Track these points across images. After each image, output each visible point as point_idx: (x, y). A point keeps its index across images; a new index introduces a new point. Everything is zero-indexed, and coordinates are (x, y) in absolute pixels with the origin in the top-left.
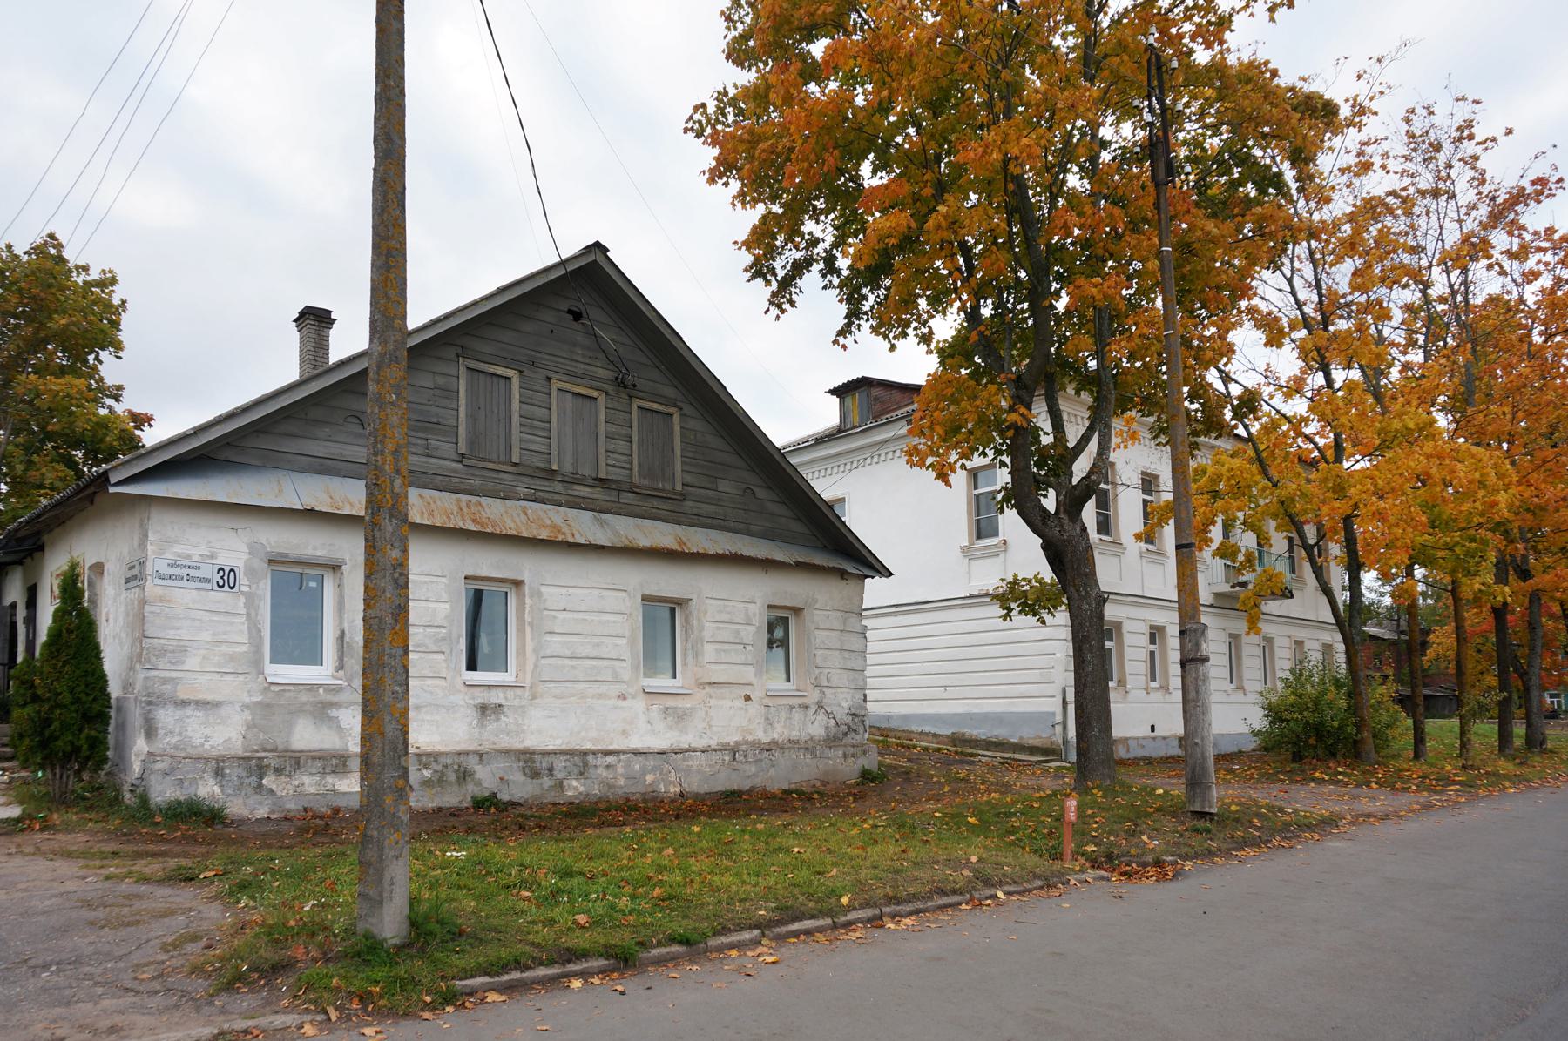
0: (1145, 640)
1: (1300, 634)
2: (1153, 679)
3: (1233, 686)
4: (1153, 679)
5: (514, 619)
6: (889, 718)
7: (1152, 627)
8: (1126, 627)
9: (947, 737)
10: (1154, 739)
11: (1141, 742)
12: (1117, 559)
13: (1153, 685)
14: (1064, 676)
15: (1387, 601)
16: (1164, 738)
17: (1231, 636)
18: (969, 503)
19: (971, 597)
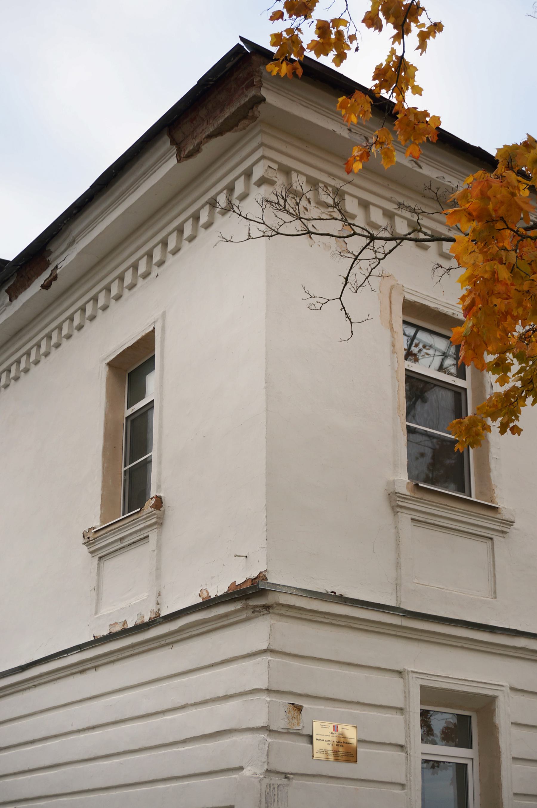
12: (482, 547)
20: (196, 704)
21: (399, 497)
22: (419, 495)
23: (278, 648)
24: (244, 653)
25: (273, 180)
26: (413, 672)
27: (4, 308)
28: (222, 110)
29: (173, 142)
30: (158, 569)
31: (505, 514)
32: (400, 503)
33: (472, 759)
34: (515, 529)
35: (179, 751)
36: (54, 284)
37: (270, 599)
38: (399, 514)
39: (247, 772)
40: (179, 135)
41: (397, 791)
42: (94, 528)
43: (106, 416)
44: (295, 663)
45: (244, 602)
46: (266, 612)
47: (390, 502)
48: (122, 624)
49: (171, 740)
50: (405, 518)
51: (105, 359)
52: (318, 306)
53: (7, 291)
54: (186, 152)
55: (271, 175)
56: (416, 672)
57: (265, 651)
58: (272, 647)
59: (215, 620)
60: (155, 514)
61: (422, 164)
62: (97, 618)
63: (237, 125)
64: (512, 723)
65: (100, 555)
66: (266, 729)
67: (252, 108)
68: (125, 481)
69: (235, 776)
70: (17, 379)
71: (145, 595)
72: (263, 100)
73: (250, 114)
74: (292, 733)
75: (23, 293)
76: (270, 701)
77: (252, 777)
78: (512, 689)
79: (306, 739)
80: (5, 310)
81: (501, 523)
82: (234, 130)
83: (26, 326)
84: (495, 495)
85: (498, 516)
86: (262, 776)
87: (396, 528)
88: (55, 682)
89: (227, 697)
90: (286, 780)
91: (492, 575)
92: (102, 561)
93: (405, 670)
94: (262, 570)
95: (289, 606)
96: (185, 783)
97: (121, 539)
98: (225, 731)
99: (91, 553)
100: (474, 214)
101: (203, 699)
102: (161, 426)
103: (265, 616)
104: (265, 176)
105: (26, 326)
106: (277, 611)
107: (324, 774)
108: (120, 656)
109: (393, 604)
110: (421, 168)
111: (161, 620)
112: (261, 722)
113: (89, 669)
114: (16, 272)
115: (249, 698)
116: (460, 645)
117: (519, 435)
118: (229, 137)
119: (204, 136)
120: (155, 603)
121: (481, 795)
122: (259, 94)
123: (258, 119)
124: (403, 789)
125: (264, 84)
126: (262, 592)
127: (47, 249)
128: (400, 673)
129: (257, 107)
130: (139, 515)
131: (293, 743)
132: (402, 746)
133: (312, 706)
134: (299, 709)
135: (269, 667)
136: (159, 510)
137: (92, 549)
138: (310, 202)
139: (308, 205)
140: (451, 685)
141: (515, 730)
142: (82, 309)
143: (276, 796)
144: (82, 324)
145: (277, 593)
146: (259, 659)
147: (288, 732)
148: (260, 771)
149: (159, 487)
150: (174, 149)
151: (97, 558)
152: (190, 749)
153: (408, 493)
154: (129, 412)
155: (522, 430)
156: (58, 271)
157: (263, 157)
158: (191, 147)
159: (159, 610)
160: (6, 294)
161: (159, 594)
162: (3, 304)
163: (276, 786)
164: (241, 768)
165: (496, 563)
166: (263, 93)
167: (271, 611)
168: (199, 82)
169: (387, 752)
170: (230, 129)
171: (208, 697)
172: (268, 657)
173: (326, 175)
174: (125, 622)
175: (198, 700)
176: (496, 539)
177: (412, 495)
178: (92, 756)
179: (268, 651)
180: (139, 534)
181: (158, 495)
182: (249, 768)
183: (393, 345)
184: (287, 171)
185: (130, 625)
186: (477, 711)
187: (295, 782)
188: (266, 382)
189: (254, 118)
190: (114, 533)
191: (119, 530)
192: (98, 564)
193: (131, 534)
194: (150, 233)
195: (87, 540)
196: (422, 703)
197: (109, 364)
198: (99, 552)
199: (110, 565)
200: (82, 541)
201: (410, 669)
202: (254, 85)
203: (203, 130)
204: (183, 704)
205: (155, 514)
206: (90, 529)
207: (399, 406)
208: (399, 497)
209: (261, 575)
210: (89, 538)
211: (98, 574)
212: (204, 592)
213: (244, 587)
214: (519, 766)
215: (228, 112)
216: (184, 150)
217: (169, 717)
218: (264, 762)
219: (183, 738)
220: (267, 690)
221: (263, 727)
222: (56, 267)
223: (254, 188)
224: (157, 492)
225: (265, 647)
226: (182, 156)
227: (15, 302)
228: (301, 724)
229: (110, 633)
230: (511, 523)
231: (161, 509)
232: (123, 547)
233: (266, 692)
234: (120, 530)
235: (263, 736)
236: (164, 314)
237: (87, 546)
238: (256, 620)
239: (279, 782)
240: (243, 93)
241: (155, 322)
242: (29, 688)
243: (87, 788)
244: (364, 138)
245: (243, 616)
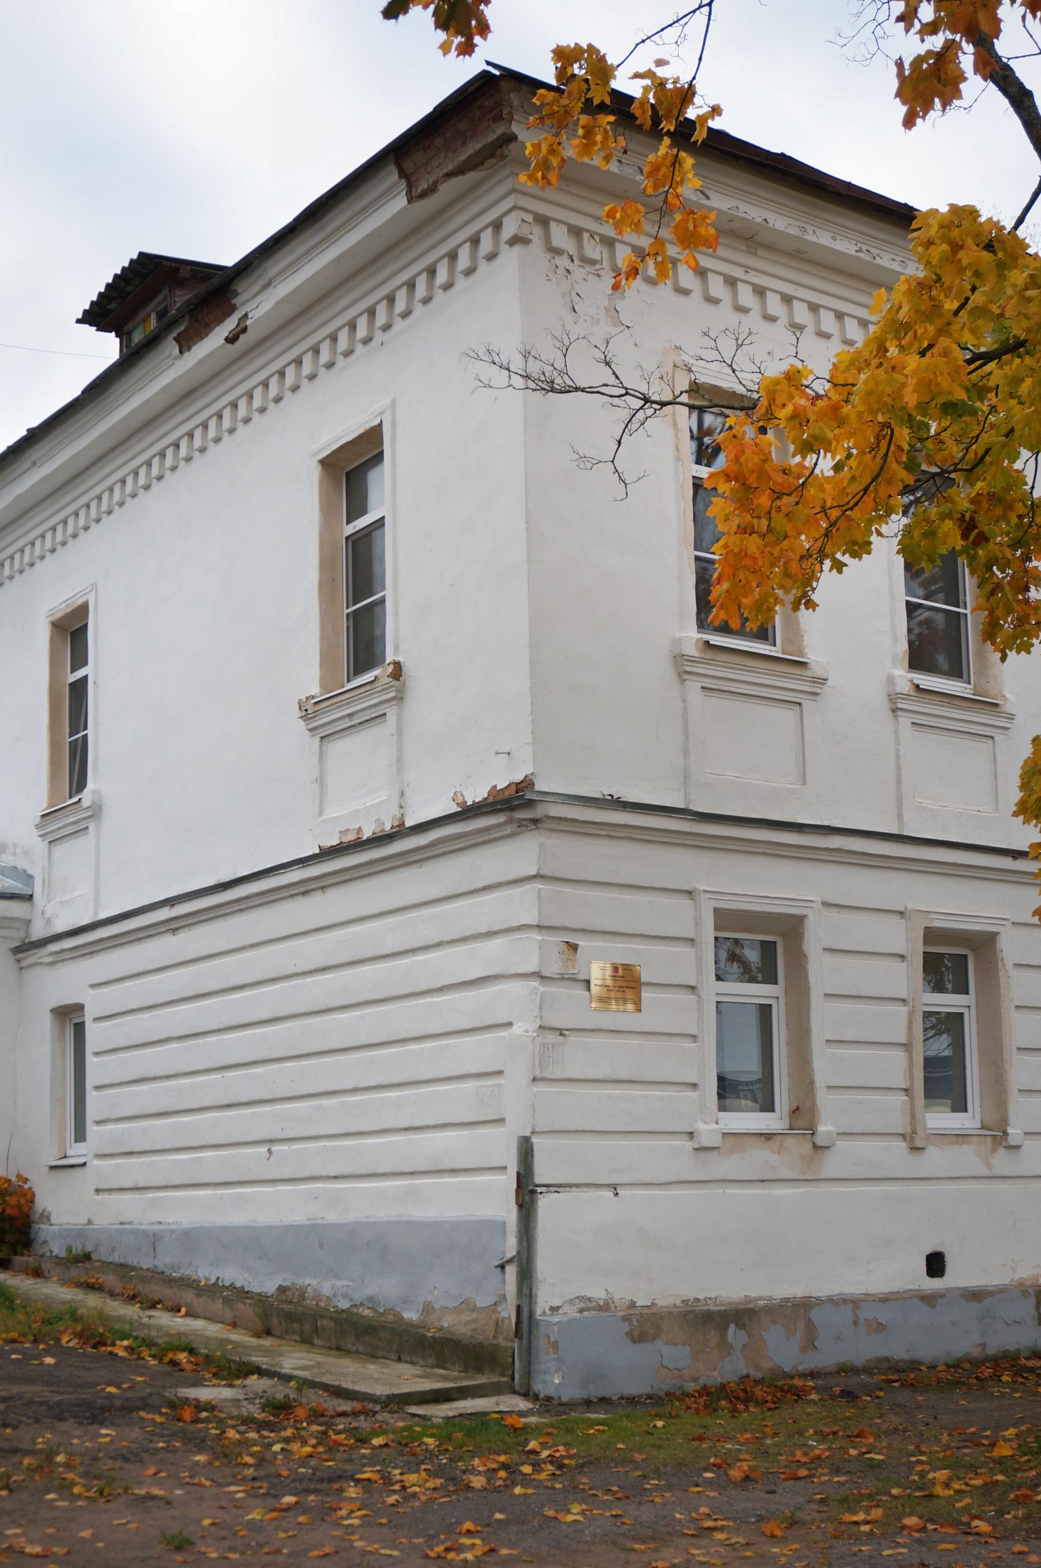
6: (154, 1240)
7: (931, 935)
9: (261, 1299)
10: (929, 1299)
11: (867, 1313)
12: (787, 716)
15: (707, 514)
16: (975, 1295)
18: (326, 565)
19: (327, 853)
20: (453, 942)
21: (687, 660)
22: (710, 655)
23: (549, 874)
24: (510, 878)
25: (527, 238)
26: (705, 891)
27: (171, 363)
28: (464, 144)
29: (403, 174)
30: (399, 760)
31: (816, 671)
32: (688, 669)
33: (777, 998)
34: (830, 687)
35: (435, 1002)
36: (242, 337)
37: (538, 812)
38: (687, 682)
39: (517, 1029)
40: (408, 166)
41: (688, 1045)
42: (313, 697)
43: (321, 535)
44: (569, 890)
45: (508, 814)
46: (534, 827)
47: (676, 666)
48: (355, 832)
49: (424, 988)
50: (694, 686)
51: (316, 454)
52: (589, 466)
53: (175, 339)
54: (419, 191)
55: (524, 233)
56: (709, 892)
57: (534, 877)
58: (542, 872)
59: (474, 834)
60: (393, 686)
61: (709, 193)
62: (323, 821)
63: (482, 163)
64: (825, 949)
65: (322, 735)
66: (538, 975)
67: (501, 146)
68: (348, 627)
69: (503, 1033)
70: (188, 459)
71: (383, 795)
72: (514, 138)
73: (498, 152)
74: (567, 979)
75: (198, 344)
76: (543, 940)
77: (523, 1035)
78: (826, 904)
79: (582, 985)
80: (173, 364)
81: (812, 682)
82: (479, 169)
83: (201, 386)
84: (805, 643)
85: (808, 673)
86: (535, 1034)
87: (684, 701)
88: (268, 906)
89: (491, 934)
90: (561, 1037)
91: (801, 753)
92: (325, 742)
93: (695, 889)
94: (529, 772)
95: (560, 819)
96: (444, 1042)
97: (350, 715)
98: (489, 976)
99: (311, 730)
100: (732, 475)
101: (462, 936)
102: (395, 563)
103: (532, 832)
104: (519, 234)
105: (201, 386)
106: (549, 826)
107: (604, 1028)
108: (355, 875)
109: (680, 805)
110: (709, 199)
111: (407, 831)
112: (532, 967)
113: (313, 890)
114: (188, 312)
115: (517, 936)
116: (761, 850)
117: (814, 611)
118: (471, 176)
119: (441, 175)
120: (397, 806)
121: (788, 1044)
122: (509, 131)
123: (508, 158)
124: (695, 1042)
125: (515, 117)
126: (530, 804)
127: (232, 288)
128: (689, 893)
129: (508, 146)
130: (373, 686)
131: (568, 991)
132: (693, 988)
133: (588, 944)
134: (574, 947)
135: (539, 897)
136: (398, 680)
137: (311, 726)
138: (572, 261)
139: (571, 264)
140: (750, 905)
141: (829, 959)
142: (279, 373)
143: (551, 1059)
144: (280, 395)
145: (546, 804)
146: (528, 886)
147: (563, 978)
148: (532, 1027)
149: (396, 648)
150: (403, 184)
151: (318, 738)
152: (448, 1000)
153: (697, 655)
154: (350, 529)
155: (818, 606)
156: (248, 322)
157: (515, 208)
158: (425, 186)
159: (402, 815)
160: (175, 343)
161: (403, 794)
162: (170, 356)
163: (550, 1046)
164: (510, 1024)
165: (806, 737)
166: (515, 128)
167: (539, 825)
168: (435, 109)
169: (676, 996)
170: (474, 168)
171: (468, 934)
172: (537, 885)
173: (592, 220)
174: (359, 830)
175: (456, 937)
176: (804, 703)
177: (702, 656)
178: (324, 1007)
179: (538, 877)
180: (373, 710)
181: (397, 659)
182: (519, 1024)
183: (677, 450)
184: (544, 221)
185: (366, 834)
186: (784, 935)
187: (573, 1039)
188: (527, 523)
189: (503, 157)
190: (340, 707)
191: (347, 704)
192: (321, 746)
193: (363, 710)
194: (370, 284)
195: (304, 713)
196: (716, 929)
197: (323, 462)
198: (321, 730)
199: (337, 748)
200: (297, 713)
201: (701, 888)
202: (504, 119)
203: (440, 164)
204: (437, 941)
205: (393, 686)
206: (307, 698)
207: (685, 534)
208: (687, 660)
209: (527, 779)
210: (306, 710)
211: (321, 759)
212: (459, 795)
213: (507, 793)
214: (832, 1004)
215: (473, 147)
216: (417, 187)
217: (420, 957)
218: (536, 1017)
219: (439, 985)
220: (538, 926)
221: (534, 973)
222: (246, 316)
223: (504, 248)
224: (394, 655)
225: (534, 872)
226: (414, 194)
227: (186, 355)
228: (577, 967)
229: (341, 843)
230: (822, 681)
231: (401, 679)
232: (353, 726)
233: (537, 928)
234: (349, 703)
235: (534, 983)
236: (393, 403)
237: (304, 721)
238: (521, 837)
239: (554, 1041)
240: (489, 126)
241: (382, 413)
242: (233, 913)
243: (319, 1050)
244: (637, 169)
245: (508, 830)
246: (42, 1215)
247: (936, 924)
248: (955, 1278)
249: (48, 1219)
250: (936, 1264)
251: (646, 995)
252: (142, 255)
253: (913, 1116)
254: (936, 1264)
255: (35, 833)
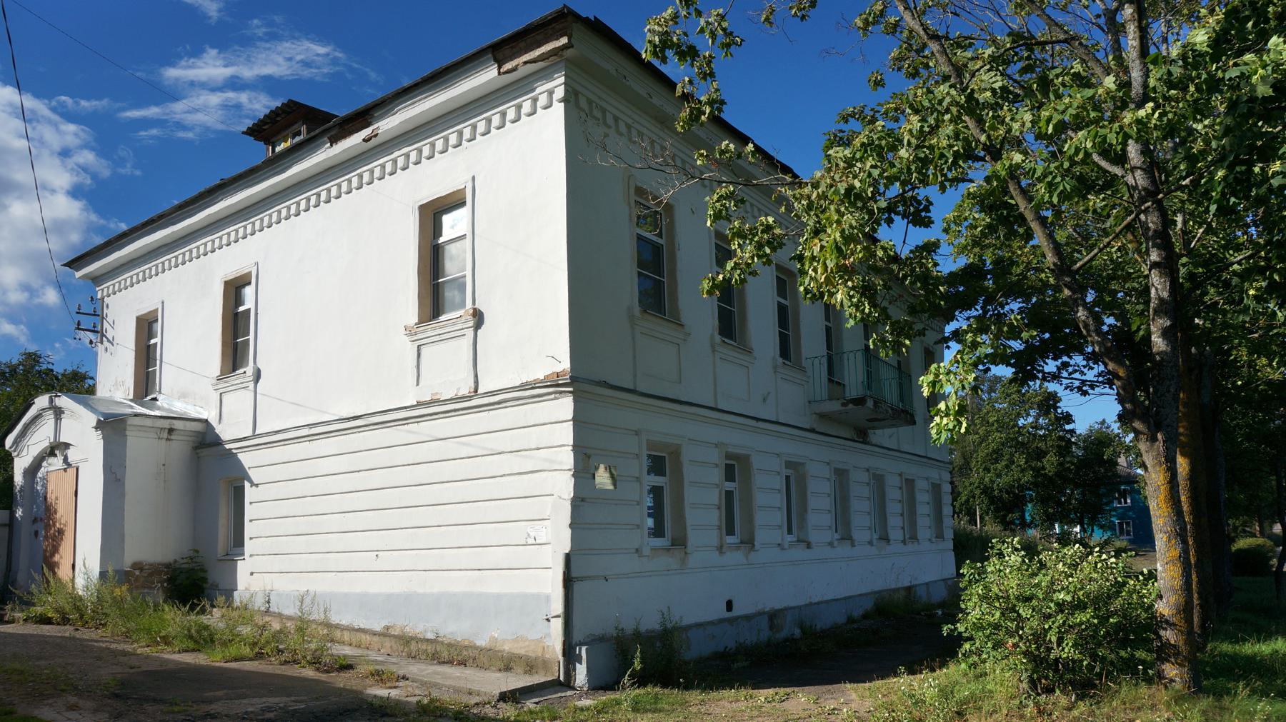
0: (717, 475)
1: (912, 470)
2: (730, 531)
3: (789, 538)
4: (730, 531)
5: (669, 507)
8: (687, 454)
10: (731, 621)
13: (730, 539)
14: (7, 535)
16: (747, 618)
17: (789, 465)
19: (420, 405)
63: (548, 59)
67: (562, 50)
227: (334, 146)
246: (212, 585)
247: (730, 450)
248: (737, 611)
249: (217, 586)
250: (729, 605)
251: (63, 439)
252: (290, 101)
253: (721, 538)
254: (729, 605)
255: (211, 388)
